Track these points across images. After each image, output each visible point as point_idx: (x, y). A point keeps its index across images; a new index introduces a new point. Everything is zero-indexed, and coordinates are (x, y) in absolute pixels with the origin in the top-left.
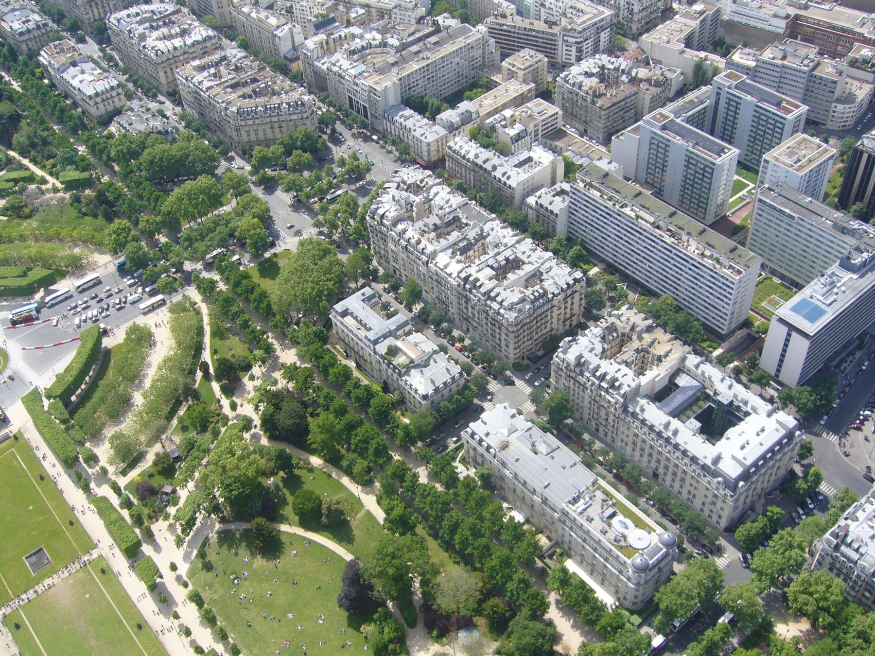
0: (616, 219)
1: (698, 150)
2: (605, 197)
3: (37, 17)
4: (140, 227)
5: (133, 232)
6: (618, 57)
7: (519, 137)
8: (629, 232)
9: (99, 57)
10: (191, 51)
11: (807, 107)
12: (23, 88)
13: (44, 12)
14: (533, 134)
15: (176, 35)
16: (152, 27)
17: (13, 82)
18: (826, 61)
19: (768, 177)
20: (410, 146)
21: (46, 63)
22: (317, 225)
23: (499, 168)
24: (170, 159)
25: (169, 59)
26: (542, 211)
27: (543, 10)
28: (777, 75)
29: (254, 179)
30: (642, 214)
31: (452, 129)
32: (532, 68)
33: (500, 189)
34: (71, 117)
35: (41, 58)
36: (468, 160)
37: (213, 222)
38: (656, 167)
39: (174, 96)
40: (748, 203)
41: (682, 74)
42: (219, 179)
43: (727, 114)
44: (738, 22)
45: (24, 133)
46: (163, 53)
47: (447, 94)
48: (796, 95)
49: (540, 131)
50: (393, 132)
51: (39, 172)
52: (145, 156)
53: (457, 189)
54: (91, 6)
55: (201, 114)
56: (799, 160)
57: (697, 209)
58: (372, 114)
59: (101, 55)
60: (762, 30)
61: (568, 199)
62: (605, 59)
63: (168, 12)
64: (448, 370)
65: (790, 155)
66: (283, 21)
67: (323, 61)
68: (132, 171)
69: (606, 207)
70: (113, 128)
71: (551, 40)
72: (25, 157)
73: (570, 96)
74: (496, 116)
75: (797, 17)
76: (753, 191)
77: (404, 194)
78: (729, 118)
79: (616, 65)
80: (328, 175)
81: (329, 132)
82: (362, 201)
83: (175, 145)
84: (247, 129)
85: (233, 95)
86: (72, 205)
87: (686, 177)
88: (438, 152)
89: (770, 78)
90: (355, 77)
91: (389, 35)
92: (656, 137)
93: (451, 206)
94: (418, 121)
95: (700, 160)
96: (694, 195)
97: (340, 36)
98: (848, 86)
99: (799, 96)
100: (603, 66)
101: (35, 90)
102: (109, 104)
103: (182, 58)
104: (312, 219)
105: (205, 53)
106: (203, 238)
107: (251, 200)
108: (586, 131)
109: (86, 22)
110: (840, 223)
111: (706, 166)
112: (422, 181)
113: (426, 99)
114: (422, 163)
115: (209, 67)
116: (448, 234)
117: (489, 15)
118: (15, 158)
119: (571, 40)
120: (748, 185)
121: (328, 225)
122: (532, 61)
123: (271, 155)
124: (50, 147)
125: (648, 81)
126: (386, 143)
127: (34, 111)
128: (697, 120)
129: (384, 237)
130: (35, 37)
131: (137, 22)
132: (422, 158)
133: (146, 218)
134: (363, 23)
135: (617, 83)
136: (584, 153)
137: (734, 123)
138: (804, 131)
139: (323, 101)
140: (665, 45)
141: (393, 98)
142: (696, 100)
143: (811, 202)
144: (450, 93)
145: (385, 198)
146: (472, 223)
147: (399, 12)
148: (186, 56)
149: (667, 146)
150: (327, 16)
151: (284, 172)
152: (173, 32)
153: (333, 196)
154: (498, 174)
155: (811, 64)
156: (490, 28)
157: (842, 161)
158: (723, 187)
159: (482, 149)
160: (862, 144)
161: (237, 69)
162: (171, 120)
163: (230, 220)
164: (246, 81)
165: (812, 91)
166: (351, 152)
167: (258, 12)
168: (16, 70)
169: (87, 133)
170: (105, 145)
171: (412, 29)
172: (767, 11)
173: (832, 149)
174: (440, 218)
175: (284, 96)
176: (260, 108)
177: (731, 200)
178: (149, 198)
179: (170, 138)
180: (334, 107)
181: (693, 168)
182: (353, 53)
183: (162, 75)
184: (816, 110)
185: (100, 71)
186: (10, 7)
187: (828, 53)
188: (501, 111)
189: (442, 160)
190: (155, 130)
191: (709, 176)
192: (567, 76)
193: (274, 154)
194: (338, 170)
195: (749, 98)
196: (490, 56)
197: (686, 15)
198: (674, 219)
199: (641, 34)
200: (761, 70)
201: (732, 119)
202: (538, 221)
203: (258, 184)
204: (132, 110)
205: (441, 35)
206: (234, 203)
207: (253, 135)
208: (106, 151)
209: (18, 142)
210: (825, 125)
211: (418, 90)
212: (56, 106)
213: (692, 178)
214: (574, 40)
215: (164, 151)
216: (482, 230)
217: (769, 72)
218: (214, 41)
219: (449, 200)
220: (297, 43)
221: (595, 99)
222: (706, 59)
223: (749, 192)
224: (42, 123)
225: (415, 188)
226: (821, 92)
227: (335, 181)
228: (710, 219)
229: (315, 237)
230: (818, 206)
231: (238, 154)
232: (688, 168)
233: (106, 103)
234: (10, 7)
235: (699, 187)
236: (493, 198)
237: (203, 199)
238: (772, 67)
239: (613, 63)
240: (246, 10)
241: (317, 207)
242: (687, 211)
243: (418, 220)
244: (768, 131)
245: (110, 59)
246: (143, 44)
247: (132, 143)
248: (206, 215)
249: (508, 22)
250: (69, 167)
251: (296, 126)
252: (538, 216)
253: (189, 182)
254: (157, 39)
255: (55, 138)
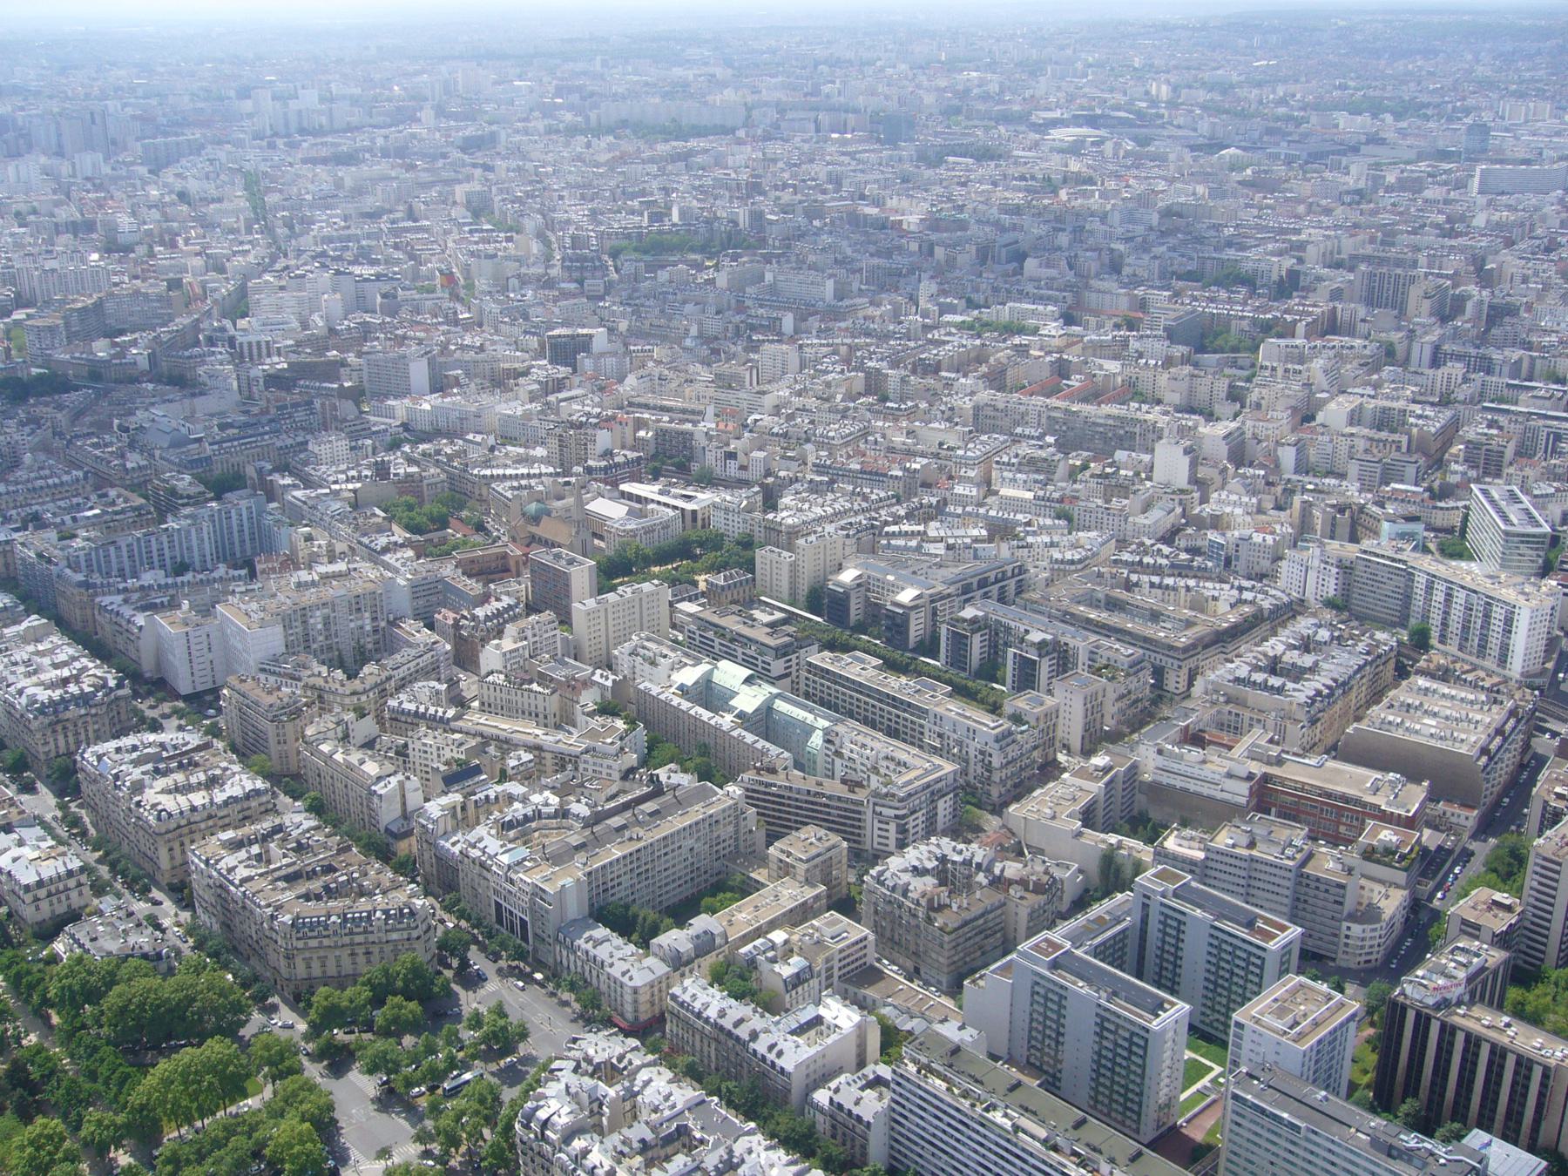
0: (978, 1132)
2: (956, 1091)
4: (83, 1133)
5: (67, 1144)
6: (969, 842)
7: (798, 980)
8: (1002, 1157)
9: (55, 818)
10: (221, 814)
11: (1299, 929)
14: (824, 975)
16: (157, 771)
18: (1324, 850)
19: (1245, 1053)
22: (421, 1138)
23: (762, 1036)
24: (158, 1006)
25: (179, 827)
26: (842, 1117)
27: (838, 761)
28: (1243, 873)
29: (310, 1047)
30: (1025, 1122)
31: (679, 963)
33: (764, 1075)
36: (707, 1020)
37: (225, 1128)
39: (182, 893)
40: (1214, 1102)
41: (1080, 871)
42: (244, 1045)
43: (1164, 942)
46: (170, 815)
50: (572, 966)
52: (113, 998)
53: (685, 1074)
54: (54, 731)
55: (227, 926)
56: (1297, 1023)
57: (1123, 1114)
58: (536, 935)
59: (59, 814)
60: (1211, 798)
61: (888, 1095)
62: (946, 845)
63: (190, 747)
65: (1281, 1012)
66: (389, 768)
67: (455, 839)
68: (84, 1026)
69: (958, 1110)
70: (59, 946)
73: (889, 908)
74: (758, 942)
75: (1266, 778)
76: (1221, 1080)
77: (588, 1082)
78: (1167, 947)
79: (967, 855)
80: (449, 1043)
81: (455, 963)
82: (508, 1094)
83: (171, 980)
84: (307, 955)
85: (288, 893)
87: (1099, 1054)
88: (653, 1004)
89: (1231, 878)
90: (509, 867)
91: (572, 798)
93: (673, 1106)
94: (618, 948)
95: (1120, 1022)
96: (1116, 1088)
97: (487, 797)
98: (1366, 893)
99: (1285, 909)
100: (944, 856)
102: (59, 901)
104: (414, 1126)
105: (245, 818)
106: (201, 1158)
107: (301, 1088)
108: (917, 970)
109: (42, 757)
110: (1383, 1138)
111: (1133, 1034)
112: (620, 1059)
113: (634, 909)
114: (623, 1024)
115: (251, 843)
116: (668, 1159)
119: (886, 812)
120: (1211, 1069)
121: (442, 1138)
122: (821, 847)
123: (345, 1003)
125: (1023, 882)
126: (558, 986)
128: (1112, 952)
129: (547, 1164)
131: (132, 762)
132: (622, 1015)
133: (97, 1115)
134: (528, 776)
135: (969, 886)
136: (915, 1010)
139: (448, 909)
140: (1049, 823)
141: (575, 907)
143: (1326, 1099)
144: (676, 900)
145: (552, 1089)
146: (711, 1139)
147: (591, 760)
148: (211, 823)
149: (1061, 997)
150: (466, 762)
151: (367, 1036)
152: (193, 780)
154: (760, 1046)
155: (1298, 856)
156: (747, 790)
157: (1372, 1024)
158: (1167, 1072)
159: (732, 1001)
160: (1403, 993)
162: (169, 934)
163: (257, 1124)
164: (314, 870)
166: (493, 1003)
170: (39, 975)
171: (614, 789)
173: (1352, 1002)
174: (654, 1129)
175: (379, 898)
176: (334, 918)
177: (1183, 1097)
178: (109, 1078)
179: (163, 966)
180: (468, 920)
181: (1111, 1037)
182: (508, 826)
183: (163, 855)
185: (51, 843)
187: (1325, 836)
189: (659, 1021)
190: (137, 952)
191: (1141, 1052)
192: (881, 873)
193: (351, 1001)
194: (468, 1035)
195: (1198, 912)
197: (1081, 773)
198: (1081, 1133)
199: (1006, 804)
202: (834, 1136)
203: (315, 1057)
204: (100, 913)
206: (268, 1092)
207: (316, 965)
208: (41, 987)
210: (1334, 960)
211: (621, 893)
213: (1110, 1055)
214: (892, 812)
215: (149, 991)
216: (730, 1152)
217: (1232, 870)
218: (264, 799)
219: (670, 1094)
221: (932, 914)
222: (1120, 846)
225: (609, 1071)
226: (1320, 903)
227: (461, 1055)
228: (1149, 1133)
229: (416, 1161)
230: (1339, 1106)
231: (285, 1001)
232: (1102, 1037)
233: (54, 899)
235: (1123, 1072)
236: (751, 1091)
237: (210, 1084)
238: (1232, 861)
239: (960, 852)
240: (325, 748)
241: (423, 1103)
242: (1106, 1118)
243: (611, 1131)
244: (1236, 970)
245: (75, 822)
246: (137, 798)
247: (90, 973)
248: (213, 1114)
249: (780, 780)
251: (396, 952)
252: (833, 1127)
253: (188, 1049)
254: (163, 792)
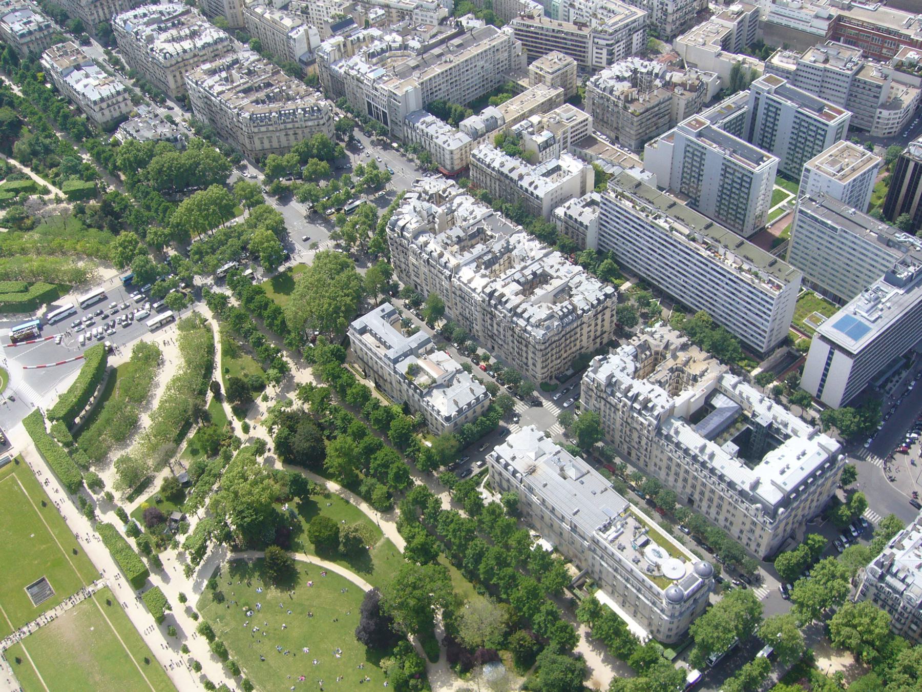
0: (649, 231)
1: (735, 158)
2: (638, 208)
3: (39, 18)
4: (147, 239)
5: (140, 245)
6: (651, 60)
7: (546, 145)
8: (663, 245)
9: (104, 60)
10: (201, 54)
11: (850, 113)
12: (24, 92)
13: (47, 13)
14: (562, 142)
15: (185, 37)
16: (160, 29)
17: (13, 87)
18: (871, 64)
19: (809, 187)
20: (432, 154)
21: (48, 66)
22: (334, 237)
23: (525, 177)
24: (180, 168)
25: (178, 62)
26: (571, 222)
27: (572, 10)
28: (819, 79)
29: (268, 188)
30: (676, 225)
31: (476, 136)
32: (560, 72)
33: (527, 199)
34: (75, 124)
35: (43, 62)
36: (493, 169)
37: (225, 234)
38: (691, 176)
39: (184, 102)
40: (788, 214)
41: (719, 78)
42: (230, 188)
43: (766, 121)
44: (777, 23)
45: (25, 140)
46: (171, 55)
47: (471, 100)
48: (839, 100)
49: (569, 138)
50: (414, 139)
51: (41, 182)
52: (153, 164)
53: (482, 200)
54: (96, 6)
55: (212, 120)
56: (842, 169)
57: (734, 221)
58: (392, 120)
59: (107, 58)
60: (803, 31)
61: (598, 210)
62: (637, 62)
63: (177, 13)
64: (472, 391)
65: (833, 163)
66: (298, 22)
67: (340, 64)
68: (139, 181)
69: (638, 219)
70: (119, 135)
71: (581, 42)
72: (26, 166)
73: (601, 101)
74: (523, 123)
75: (840, 18)
76: (794, 202)
77: (426, 205)
78: (768, 124)
79: (650, 68)
80: (346, 184)
81: (346, 139)
82: (381, 212)
83: (185, 153)
84: (260, 136)
85: (246, 100)
86: (75, 216)
87: (722, 186)
88: (462, 160)
89: (811, 82)
90: (374, 81)
91: (409, 37)
92: (692, 145)
93: (475, 218)
94: (441, 128)
95: (737, 168)
96: (731, 206)
97: (358, 38)
98: (894, 91)
99: (842, 101)
100: (636, 69)
101: (36, 95)
102: (115, 110)
103: (191, 61)
104: (329, 231)
105: (216, 56)
107: (265, 211)
108: (617, 138)
109: (91, 23)
110: (885, 235)
111: (744, 175)
112: (444, 191)
113: (449, 104)
114: (445, 172)
115: (221, 71)
116: (473, 246)
117: (515, 16)
118: (16, 167)
119: (601, 42)
120: (788, 195)
121: (345, 237)
122: (561, 65)
123: (285, 163)
124: (52, 155)
125: (683, 85)
126: (406, 151)
127: (36, 117)
128: (734, 127)
129: (405, 250)
130: (36, 39)
131: (145, 23)
132: (444, 167)
133: (154, 230)
134: (382, 24)
135: (650, 87)
136: (615, 162)
137: (773, 130)
138: (848, 139)
139: (340, 107)
140: (701, 48)
141: (414, 104)
142: (733, 106)
143: (855, 213)
144: (474, 98)
145: (406, 209)
146: (497, 235)
147: (420, 13)
148: (196, 59)
149: (703, 154)
150: (344, 17)
151: (299, 182)
152: (182, 33)
153: (351, 207)
154: (525, 183)
155: (854, 68)
156: (516, 30)
157: (888, 170)
158: (762, 197)
159: (508, 158)
160: (909, 152)
161: (250, 73)
162: (180, 127)
163: (242, 232)
164: (259, 86)
165: (856, 96)
166: (369, 161)
167: (272, 13)
168: (16, 74)
169: (91, 141)
170: (110, 153)
171: (435, 31)
172: (808, 12)
173: (877, 157)
174: (464, 230)
175: (299, 101)
176: (274, 114)
177: (770, 211)
178: (157, 209)
179: (179, 146)
180: (352, 113)
181: (731, 177)
182: (372, 55)
183: (170, 79)
184: (860, 117)
185: (106, 75)
186: (11, 8)
187: (873, 55)
188: (528, 117)
189: (466, 169)
190: (163, 138)
191: (747, 186)
192: (597, 80)
193: (288, 162)
194: (356, 180)
195: (789, 103)
196: (517, 59)
197: (723, 16)
198: (710, 231)
199: (675, 36)
200: (801, 73)
201: (771, 125)
202: (567, 234)
203: (271, 194)
204: (139, 116)
205: (464, 37)
206: (246, 214)
207: (266, 142)
208: (112, 160)
209: (19, 149)
210: (869, 132)
211: (441, 95)
212: (59, 112)
213: (729, 187)
214: (605, 42)
215: (173, 160)
216: (508, 242)
217: (810, 76)
218: (226, 43)
219: (473, 211)
220: (313, 46)
221: (627, 105)
222: (744, 62)
223: (789, 202)
224: (44, 130)
225: (438, 199)
226: (865, 97)
227: (353, 191)
228: (749, 231)
229: (332, 250)
230: (862, 217)
231: (250, 163)
232: (725, 177)
233: (112, 108)
234: (11, 8)
235: (736, 197)
236: (520, 209)
237: (214, 210)
238: (813, 71)
239: (646, 67)
240: (259, 10)
241: (334, 218)
242: (724, 223)
243: (440, 232)
244: (809, 138)
245: (116, 62)
246: (151, 46)
247: (139, 151)
248: (217, 227)
249: (536, 23)
250: (73, 176)
251: (312, 133)
252: (567, 228)
253: (199, 191)
254: (165, 41)
255: (58, 146)
